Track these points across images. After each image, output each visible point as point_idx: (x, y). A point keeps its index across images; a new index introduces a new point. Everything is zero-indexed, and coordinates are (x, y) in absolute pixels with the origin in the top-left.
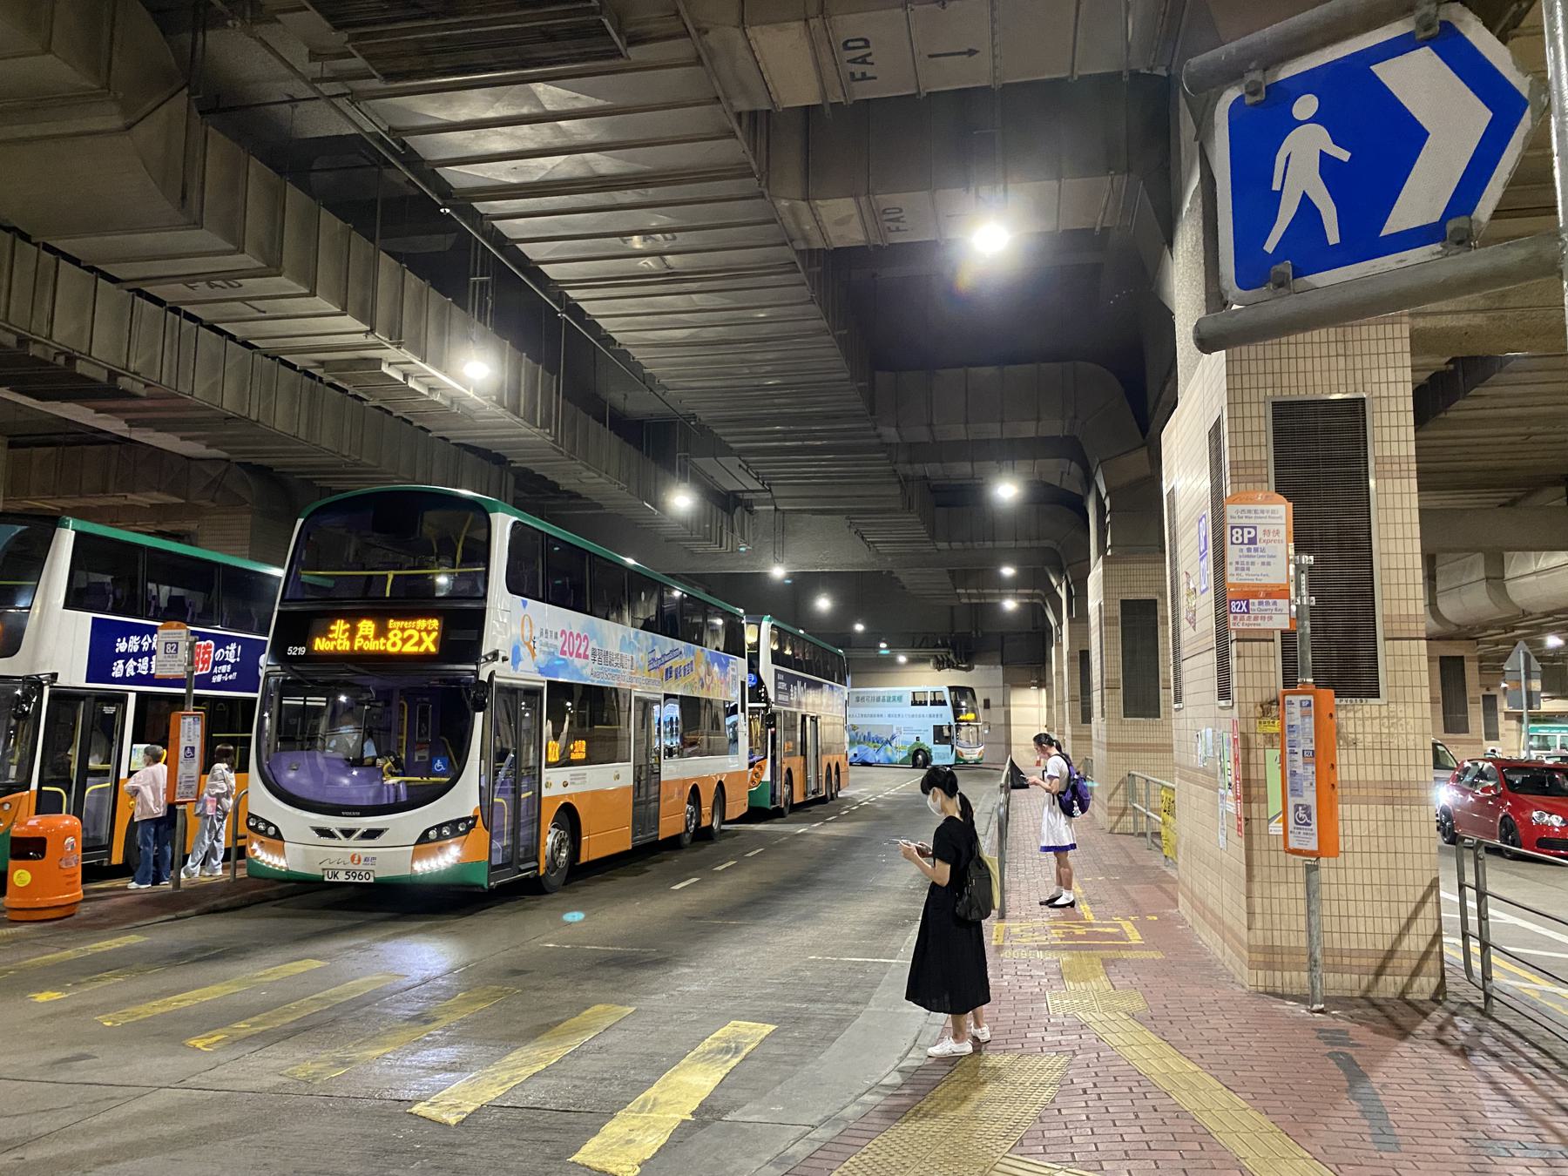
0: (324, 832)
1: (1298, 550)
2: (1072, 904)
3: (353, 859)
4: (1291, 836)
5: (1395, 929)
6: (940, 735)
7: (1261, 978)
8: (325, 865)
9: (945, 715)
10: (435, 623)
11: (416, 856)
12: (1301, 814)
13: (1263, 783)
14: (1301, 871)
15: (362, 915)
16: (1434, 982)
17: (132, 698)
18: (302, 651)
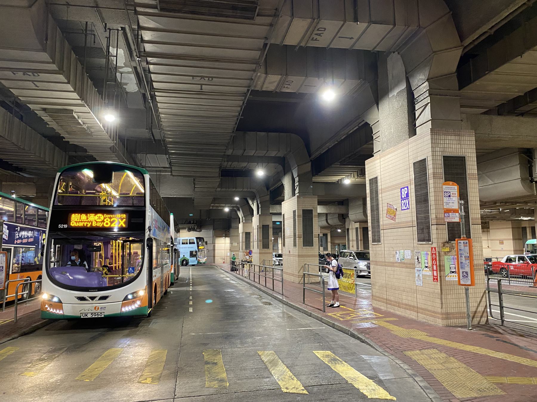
0: (82, 299)
1: (461, 199)
2: (339, 306)
3: (95, 308)
4: (461, 281)
5: (477, 305)
6: (192, 254)
7: (445, 322)
8: (81, 312)
9: (194, 247)
10: (124, 216)
11: (123, 305)
12: (464, 274)
13: (444, 266)
14: (464, 291)
15: (98, 330)
16: (486, 319)
17: (13, 248)
18: (66, 226)
